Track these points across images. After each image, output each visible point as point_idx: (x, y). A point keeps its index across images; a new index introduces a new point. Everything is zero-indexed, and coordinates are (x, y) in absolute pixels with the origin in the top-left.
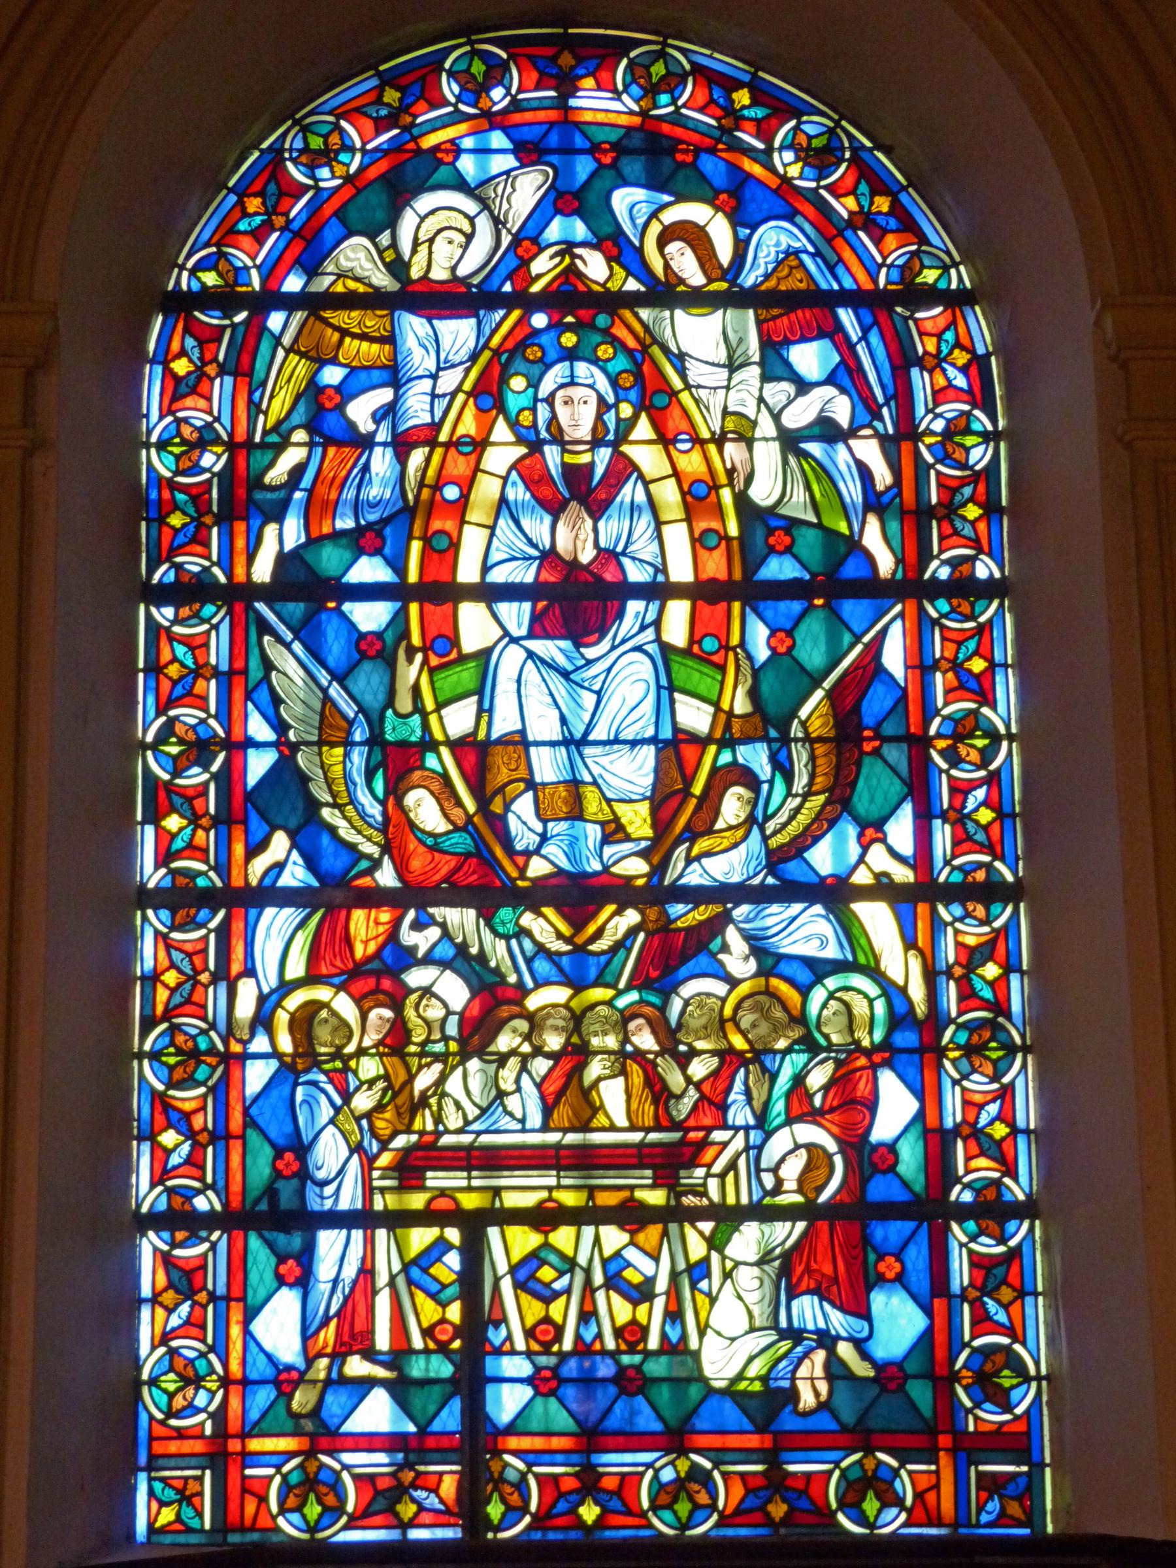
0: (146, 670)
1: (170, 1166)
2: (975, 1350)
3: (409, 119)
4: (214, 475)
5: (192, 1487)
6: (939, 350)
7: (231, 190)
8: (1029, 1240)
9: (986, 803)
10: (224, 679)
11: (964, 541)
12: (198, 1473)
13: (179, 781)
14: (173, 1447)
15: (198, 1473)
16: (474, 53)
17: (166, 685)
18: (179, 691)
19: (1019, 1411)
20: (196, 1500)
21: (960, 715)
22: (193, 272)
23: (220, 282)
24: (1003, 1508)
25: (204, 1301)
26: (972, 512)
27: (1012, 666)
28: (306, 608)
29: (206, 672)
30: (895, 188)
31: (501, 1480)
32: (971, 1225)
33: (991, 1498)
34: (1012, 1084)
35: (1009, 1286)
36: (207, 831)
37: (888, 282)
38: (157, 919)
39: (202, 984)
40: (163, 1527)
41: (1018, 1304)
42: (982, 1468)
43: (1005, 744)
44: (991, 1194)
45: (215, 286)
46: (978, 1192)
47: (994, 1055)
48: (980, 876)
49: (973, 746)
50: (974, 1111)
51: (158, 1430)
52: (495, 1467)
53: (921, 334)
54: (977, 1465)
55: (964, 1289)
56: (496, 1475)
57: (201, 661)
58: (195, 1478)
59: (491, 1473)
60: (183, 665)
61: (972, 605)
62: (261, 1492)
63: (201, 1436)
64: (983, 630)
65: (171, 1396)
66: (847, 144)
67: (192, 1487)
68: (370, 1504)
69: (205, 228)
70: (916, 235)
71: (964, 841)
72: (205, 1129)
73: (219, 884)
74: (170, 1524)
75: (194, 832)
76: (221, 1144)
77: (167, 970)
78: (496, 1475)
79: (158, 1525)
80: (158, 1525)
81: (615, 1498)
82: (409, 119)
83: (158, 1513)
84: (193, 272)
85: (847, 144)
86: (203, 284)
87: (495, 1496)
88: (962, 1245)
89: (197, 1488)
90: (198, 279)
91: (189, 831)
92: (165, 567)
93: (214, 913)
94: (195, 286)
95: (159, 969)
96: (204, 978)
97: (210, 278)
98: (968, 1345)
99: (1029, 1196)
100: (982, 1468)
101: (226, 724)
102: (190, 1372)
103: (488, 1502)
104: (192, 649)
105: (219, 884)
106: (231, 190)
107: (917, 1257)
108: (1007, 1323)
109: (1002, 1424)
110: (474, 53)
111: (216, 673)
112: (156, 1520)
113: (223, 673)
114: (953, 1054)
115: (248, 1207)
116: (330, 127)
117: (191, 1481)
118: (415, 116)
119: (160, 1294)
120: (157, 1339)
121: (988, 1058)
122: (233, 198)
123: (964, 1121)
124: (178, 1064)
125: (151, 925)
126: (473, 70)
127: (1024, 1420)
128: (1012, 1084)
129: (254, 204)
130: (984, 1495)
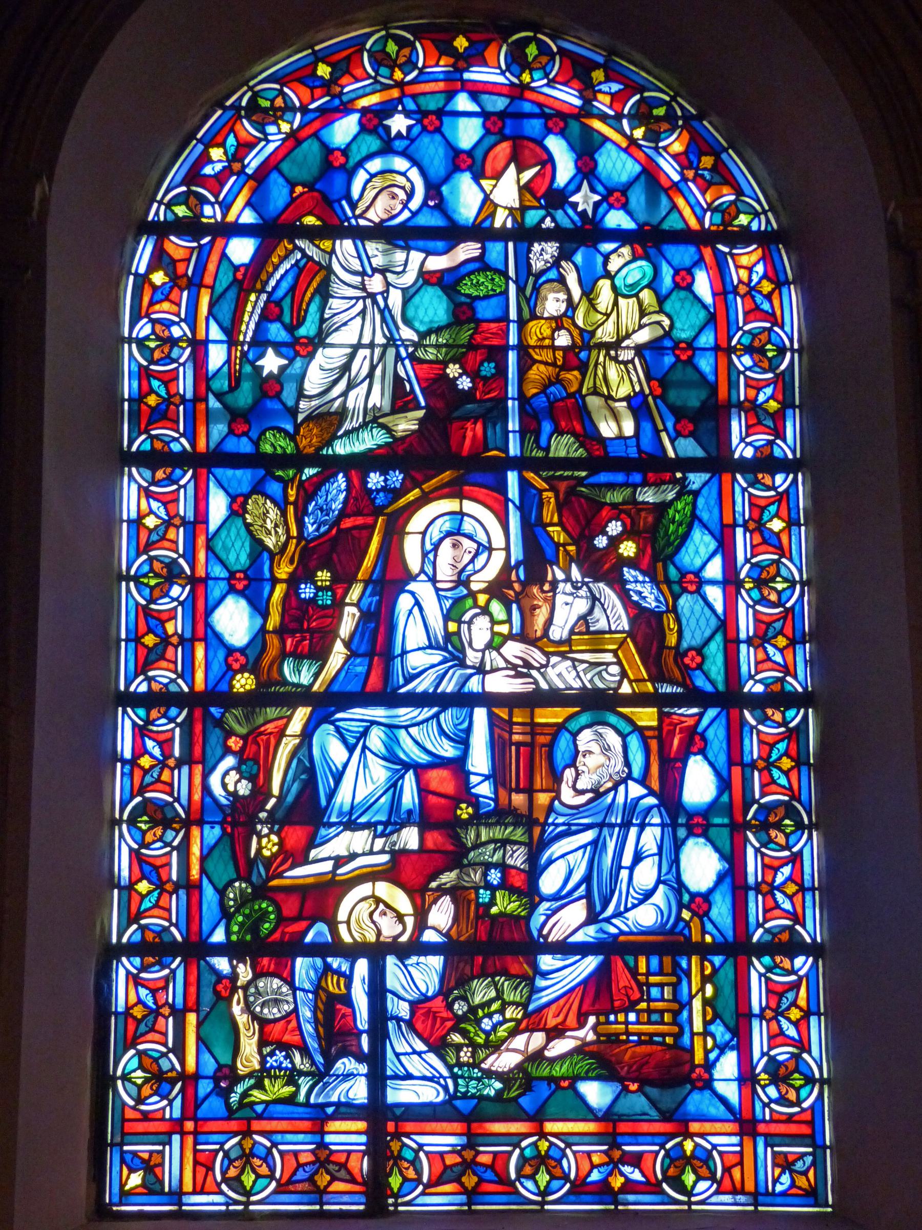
0: (127, 640)
1: (142, 908)
2: (762, 806)
3: (338, 89)
4: (173, 848)
5: (156, 1160)
6: (750, 280)
7: (199, 141)
8: (819, 1103)
9: (787, 754)
10: (190, 527)
11: (779, 790)
12: (160, 1148)
13: (153, 606)
14: (141, 1127)
15: (160, 1148)
16: (389, 36)
17: (142, 652)
18: (142, 1028)
19: (805, 1105)
20: (158, 1171)
21: (757, 331)
22: (169, 206)
23: (189, 214)
24: (793, 1181)
25: (172, 765)
26: (786, 763)
27: (794, 282)
28: (253, 476)
29: (177, 521)
30: (718, 149)
31: (400, 1157)
32: (767, 960)
33: (783, 1172)
34: (801, 852)
35: (784, 636)
36: (172, 770)
37: (711, 224)
38: (139, 476)
39: (164, 1016)
40: (132, 1189)
41: (800, 896)
42: (776, 1149)
43: (788, 355)
44: (777, 688)
45: (184, 217)
46: (767, 686)
47: (770, 354)
48: (785, 937)
49: (775, 589)
50: (771, 872)
51: (130, 1114)
52: (395, 1146)
53: (737, 267)
54: (772, 1146)
55: (762, 1010)
56: (396, 1153)
57: (172, 514)
58: (158, 1152)
59: (392, 1152)
60: (158, 517)
61: (783, 713)
62: (209, 1164)
63: (163, 1119)
64: (783, 497)
65: (144, 833)
66: (679, 113)
67: (156, 1160)
68: (294, 1173)
69: (177, 171)
70: (732, 187)
71: (777, 1035)
72: (176, 633)
73: (186, 689)
74: (137, 1187)
75: (160, 895)
76: (194, 289)
77: (147, 634)
78: (396, 1153)
79: (127, 1188)
80: (127, 1188)
81: (489, 1171)
82: (338, 89)
83: (128, 1178)
84: (169, 206)
85: (679, 113)
86: (176, 215)
87: (396, 1170)
88: (760, 975)
89: (159, 1160)
90: (173, 212)
91: (156, 894)
92: (143, 437)
93: (185, 473)
94: (170, 217)
95: (143, 393)
96: (171, 762)
97: (181, 211)
98: (741, 329)
99: (805, 688)
100: (776, 1149)
101: (191, 561)
102: (159, 816)
103: (390, 1175)
104: (165, 504)
105: (186, 689)
106: (199, 141)
107: (717, 736)
108: (782, 663)
109: (791, 1115)
110: (389, 36)
111: (184, 522)
112: (126, 1183)
113: (189, 522)
114: (747, 586)
115: (210, 687)
116: (276, 93)
117: (155, 1155)
118: (343, 87)
119: (132, 1007)
120: (142, 547)
121: (793, 1086)
122: (200, 147)
123: (763, 881)
124: (157, 585)
125: (136, 482)
126: (388, 49)
127: (809, 1112)
128: (801, 852)
129: (216, 153)
130: (778, 1171)
